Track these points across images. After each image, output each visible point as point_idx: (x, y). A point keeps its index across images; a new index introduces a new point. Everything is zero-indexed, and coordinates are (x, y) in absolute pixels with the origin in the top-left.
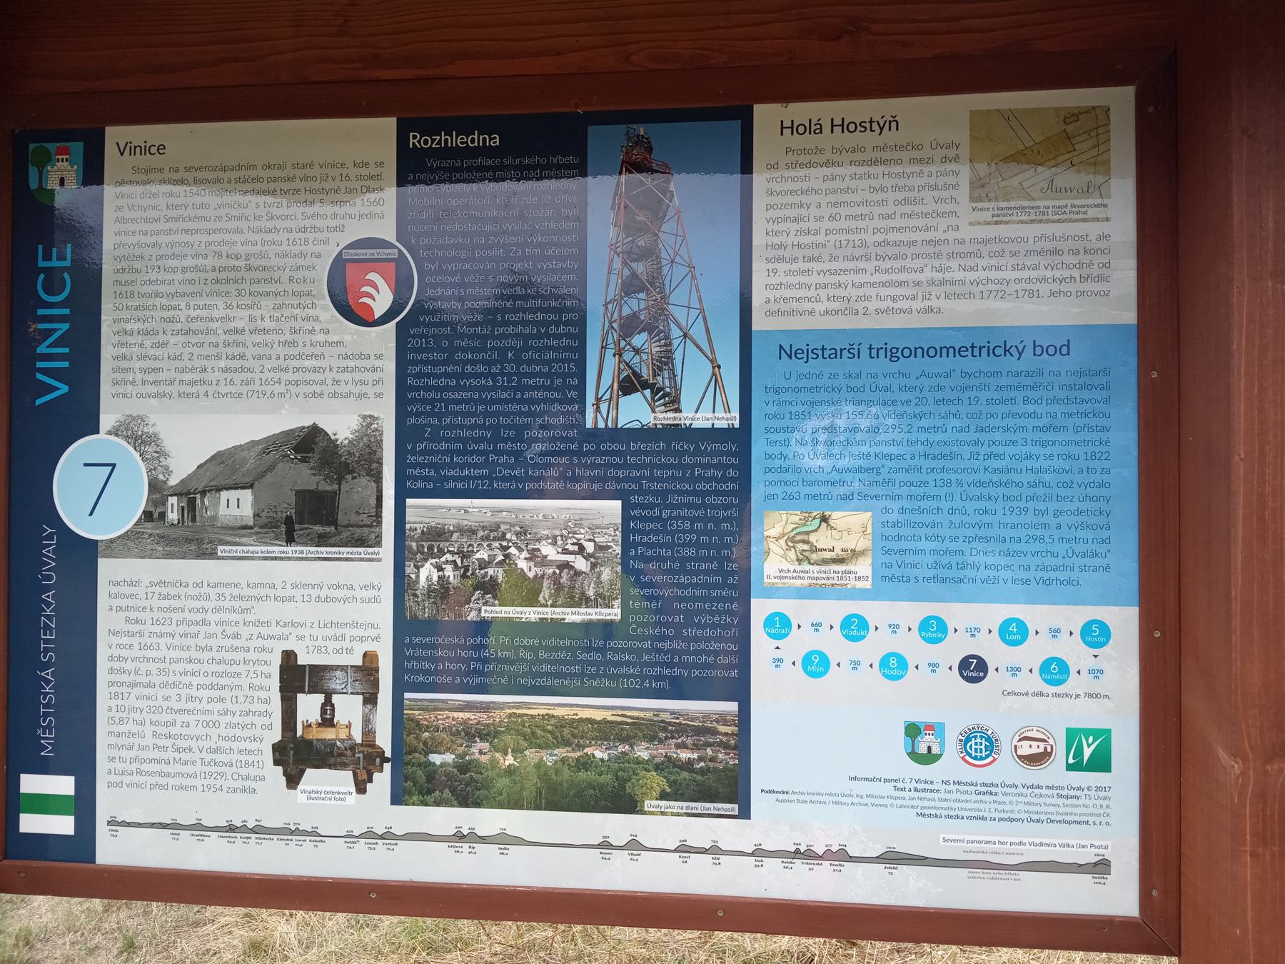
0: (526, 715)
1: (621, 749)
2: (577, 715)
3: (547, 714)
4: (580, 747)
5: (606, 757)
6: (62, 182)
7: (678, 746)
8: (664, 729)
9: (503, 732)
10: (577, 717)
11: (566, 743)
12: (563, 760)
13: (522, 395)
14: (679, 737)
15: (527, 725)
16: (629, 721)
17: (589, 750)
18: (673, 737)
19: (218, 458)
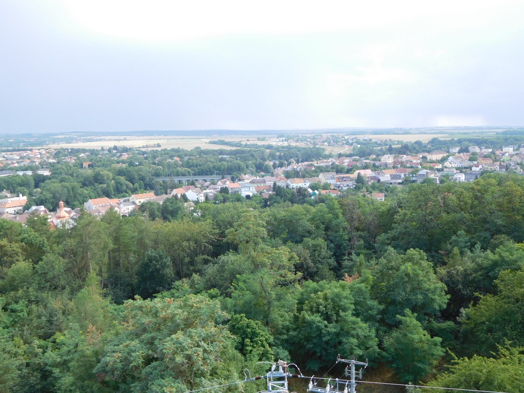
0: (84, 151)
1: (220, 185)
2: (159, 146)
3: (115, 148)
4: (165, 189)
5: (202, 199)
6: (424, 335)
7: (288, 175)
8: (272, 156)
9: (347, 240)
10: (159, 149)
11: (148, 186)
12: (142, 208)
13: (280, 154)
14: (289, 164)
15: (85, 165)
16: (228, 148)
17: (178, 192)
18: (281, 165)
19: (173, 149)
